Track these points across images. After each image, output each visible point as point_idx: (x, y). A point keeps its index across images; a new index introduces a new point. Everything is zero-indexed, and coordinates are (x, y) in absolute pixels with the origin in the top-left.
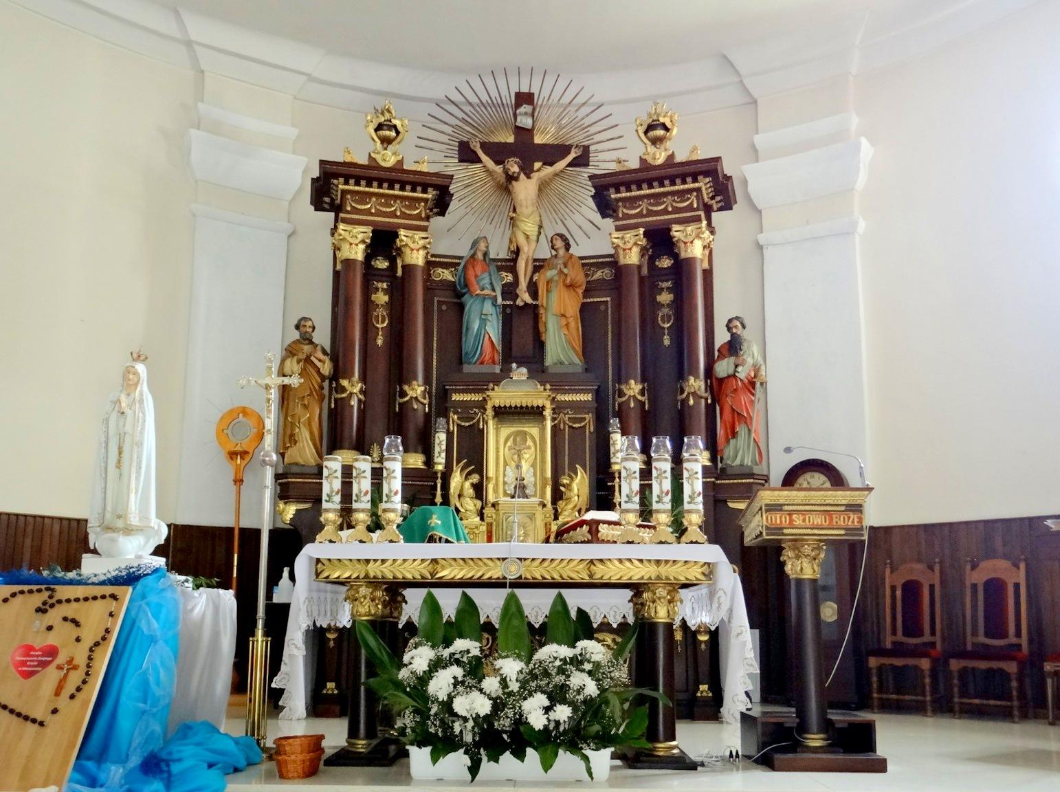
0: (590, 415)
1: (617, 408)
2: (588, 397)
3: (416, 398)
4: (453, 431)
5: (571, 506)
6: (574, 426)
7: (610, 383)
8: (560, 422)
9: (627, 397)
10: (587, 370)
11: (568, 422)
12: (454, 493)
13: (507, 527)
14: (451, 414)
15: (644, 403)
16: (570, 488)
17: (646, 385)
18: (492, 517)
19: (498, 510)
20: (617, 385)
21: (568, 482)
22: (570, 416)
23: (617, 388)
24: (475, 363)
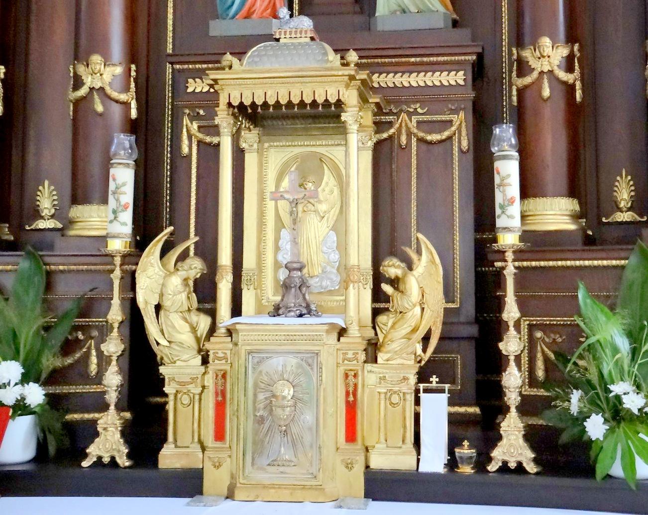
0: (462, 114)
1: (515, 99)
2: (458, 78)
3: (102, 89)
4: (189, 156)
5: (405, 329)
6: (429, 138)
7: (505, 49)
8: (399, 130)
9: (535, 75)
10: (455, 24)
11: (415, 131)
12: (146, 303)
13: (256, 386)
14: (186, 120)
15: (571, 88)
16: (401, 287)
17: (576, 47)
18: (225, 358)
19: (236, 344)
20: (514, 51)
21: (399, 272)
22: (421, 118)
23: (515, 57)
24: (233, 17)
